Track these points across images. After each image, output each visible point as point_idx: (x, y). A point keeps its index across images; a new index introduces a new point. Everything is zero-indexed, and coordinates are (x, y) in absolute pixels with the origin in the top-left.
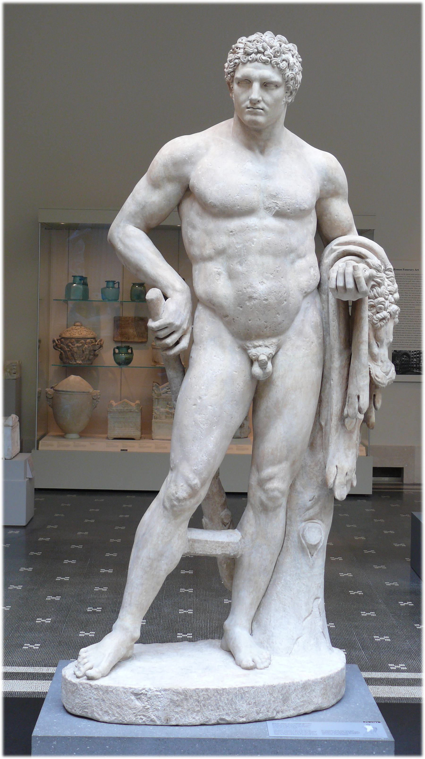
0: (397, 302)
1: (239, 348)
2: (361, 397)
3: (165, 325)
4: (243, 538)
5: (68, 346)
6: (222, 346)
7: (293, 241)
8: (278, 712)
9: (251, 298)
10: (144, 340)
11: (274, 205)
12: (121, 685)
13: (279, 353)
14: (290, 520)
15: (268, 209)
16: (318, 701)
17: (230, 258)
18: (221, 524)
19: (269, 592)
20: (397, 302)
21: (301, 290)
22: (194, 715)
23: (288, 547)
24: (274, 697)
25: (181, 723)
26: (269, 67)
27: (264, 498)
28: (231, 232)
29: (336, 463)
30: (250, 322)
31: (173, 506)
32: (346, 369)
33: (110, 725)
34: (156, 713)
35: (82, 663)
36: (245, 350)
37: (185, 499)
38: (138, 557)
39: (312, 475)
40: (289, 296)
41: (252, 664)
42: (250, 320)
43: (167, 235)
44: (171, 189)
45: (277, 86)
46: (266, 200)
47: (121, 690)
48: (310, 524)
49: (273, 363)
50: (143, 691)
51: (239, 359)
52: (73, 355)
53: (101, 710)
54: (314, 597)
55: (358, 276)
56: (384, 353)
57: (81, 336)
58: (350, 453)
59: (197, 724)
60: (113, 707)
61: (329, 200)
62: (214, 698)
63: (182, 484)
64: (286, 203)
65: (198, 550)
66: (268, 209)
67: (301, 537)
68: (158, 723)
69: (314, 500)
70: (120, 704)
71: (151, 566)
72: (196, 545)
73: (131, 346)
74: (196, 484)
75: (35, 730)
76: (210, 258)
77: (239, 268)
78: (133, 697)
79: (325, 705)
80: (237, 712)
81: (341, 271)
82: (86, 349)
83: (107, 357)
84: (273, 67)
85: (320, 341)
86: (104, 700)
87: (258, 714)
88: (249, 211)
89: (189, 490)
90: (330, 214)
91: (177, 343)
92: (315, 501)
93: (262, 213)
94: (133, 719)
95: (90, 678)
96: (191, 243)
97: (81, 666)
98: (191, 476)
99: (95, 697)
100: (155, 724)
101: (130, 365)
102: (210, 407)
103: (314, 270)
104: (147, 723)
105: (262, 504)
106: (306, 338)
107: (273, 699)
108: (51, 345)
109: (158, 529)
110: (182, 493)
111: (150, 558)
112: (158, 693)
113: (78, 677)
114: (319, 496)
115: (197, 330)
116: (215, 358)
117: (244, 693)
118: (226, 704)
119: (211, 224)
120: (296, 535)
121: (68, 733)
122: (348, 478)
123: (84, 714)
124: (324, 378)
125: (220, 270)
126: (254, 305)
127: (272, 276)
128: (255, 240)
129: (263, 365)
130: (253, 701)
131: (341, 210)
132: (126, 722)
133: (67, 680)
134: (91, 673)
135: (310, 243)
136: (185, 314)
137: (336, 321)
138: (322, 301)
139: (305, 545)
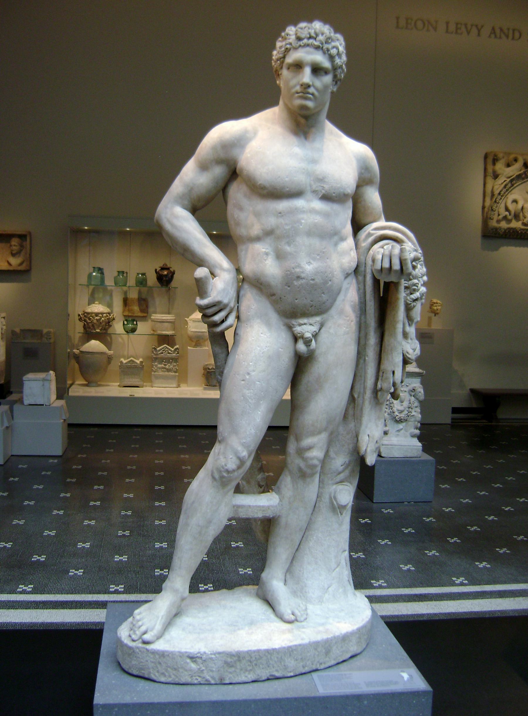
0: (424, 284)
1: (284, 325)
2: (396, 372)
3: (213, 303)
4: (281, 500)
5: (90, 319)
6: (268, 324)
7: (337, 223)
8: (321, 664)
9: (299, 278)
10: (145, 315)
11: (321, 188)
12: (177, 650)
13: (322, 331)
14: (323, 483)
15: (314, 192)
16: (354, 649)
17: (279, 238)
18: (257, 486)
19: (301, 546)
20: (424, 284)
21: (343, 270)
22: (247, 673)
23: (319, 507)
24: (318, 652)
25: (234, 682)
26: (320, 52)
27: (302, 465)
28: (280, 213)
29: (368, 432)
30: (296, 301)
31: (222, 477)
32: (379, 346)
33: (167, 685)
34: (211, 674)
35: (137, 625)
36: (290, 328)
37: (234, 471)
38: (187, 524)
39: (344, 442)
40: (333, 277)
41: (293, 618)
42: (296, 299)
43: (210, 208)
44: (219, 171)
45: (326, 72)
46: (312, 183)
47: (177, 654)
48: (340, 487)
49: (316, 341)
50: (199, 655)
51: (284, 336)
52: (93, 326)
53: (158, 672)
54: (342, 550)
55: (405, 257)
56: (412, 330)
57: (99, 311)
58: (380, 423)
59: (249, 681)
60: (169, 669)
61: (365, 187)
62: (265, 658)
63: (231, 456)
64: (332, 187)
65: (241, 514)
66: (314, 192)
67: (333, 499)
68: (213, 682)
69: (345, 465)
70: (176, 667)
71: (200, 533)
72: (240, 510)
73: (136, 319)
74: (245, 456)
75: (95, 695)
76: (258, 239)
77: (288, 249)
78: (188, 660)
79: (359, 651)
80: (286, 668)
81: (387, 253)
82: (103, 321)
83: (118, 327)
84: (324, 53)
85: (358, 319)
86: (160, 663)
87: (304, 667)
88: (297, 194)
89: (238, 462)
90: (365, 201)
91: (223, 322)
92: (347, 466)
93: (309, 195)
94: (189, 680)
95: (145, 642)
96: (238, 224)
97: (136, 629)
98: (240, 448)
99: (152, 660)
100: (209, 683)
101: (135, 333)
102: (258, 383)
103: (354, 252)
104: (202, 683)
105: (300, 470)
106: (347, 317)
107: (317, 653)
108: (77, 318)
109: (207, 498)
110: (232, 464)
111: (199, 526)
112: (213, 656)
113: (134, 641)
114: (350, 462)
115: (243, 308)
116: (262, 335)
117: (292, 651)
118: (275, 662)
119: (261, 205)
120: (327, 497)
121: (128, 699)
122: (377, 445)
123: (141, 675)
124: (360, 354)
125: (267, 251)
126: (302, 284)
127: (318, 257)
128: (303, 221)
129: (307, 342)
130: (300, 657)
131: (374, 197)
132: (182, 683)
133: (123, 642)
134: (146, 637)
135: (349, 229)
136: (232, 293)
137: (373, 301)
138: (358, 283)
139: (337, 506)
